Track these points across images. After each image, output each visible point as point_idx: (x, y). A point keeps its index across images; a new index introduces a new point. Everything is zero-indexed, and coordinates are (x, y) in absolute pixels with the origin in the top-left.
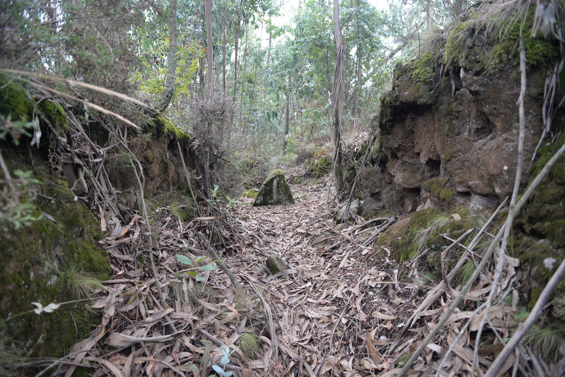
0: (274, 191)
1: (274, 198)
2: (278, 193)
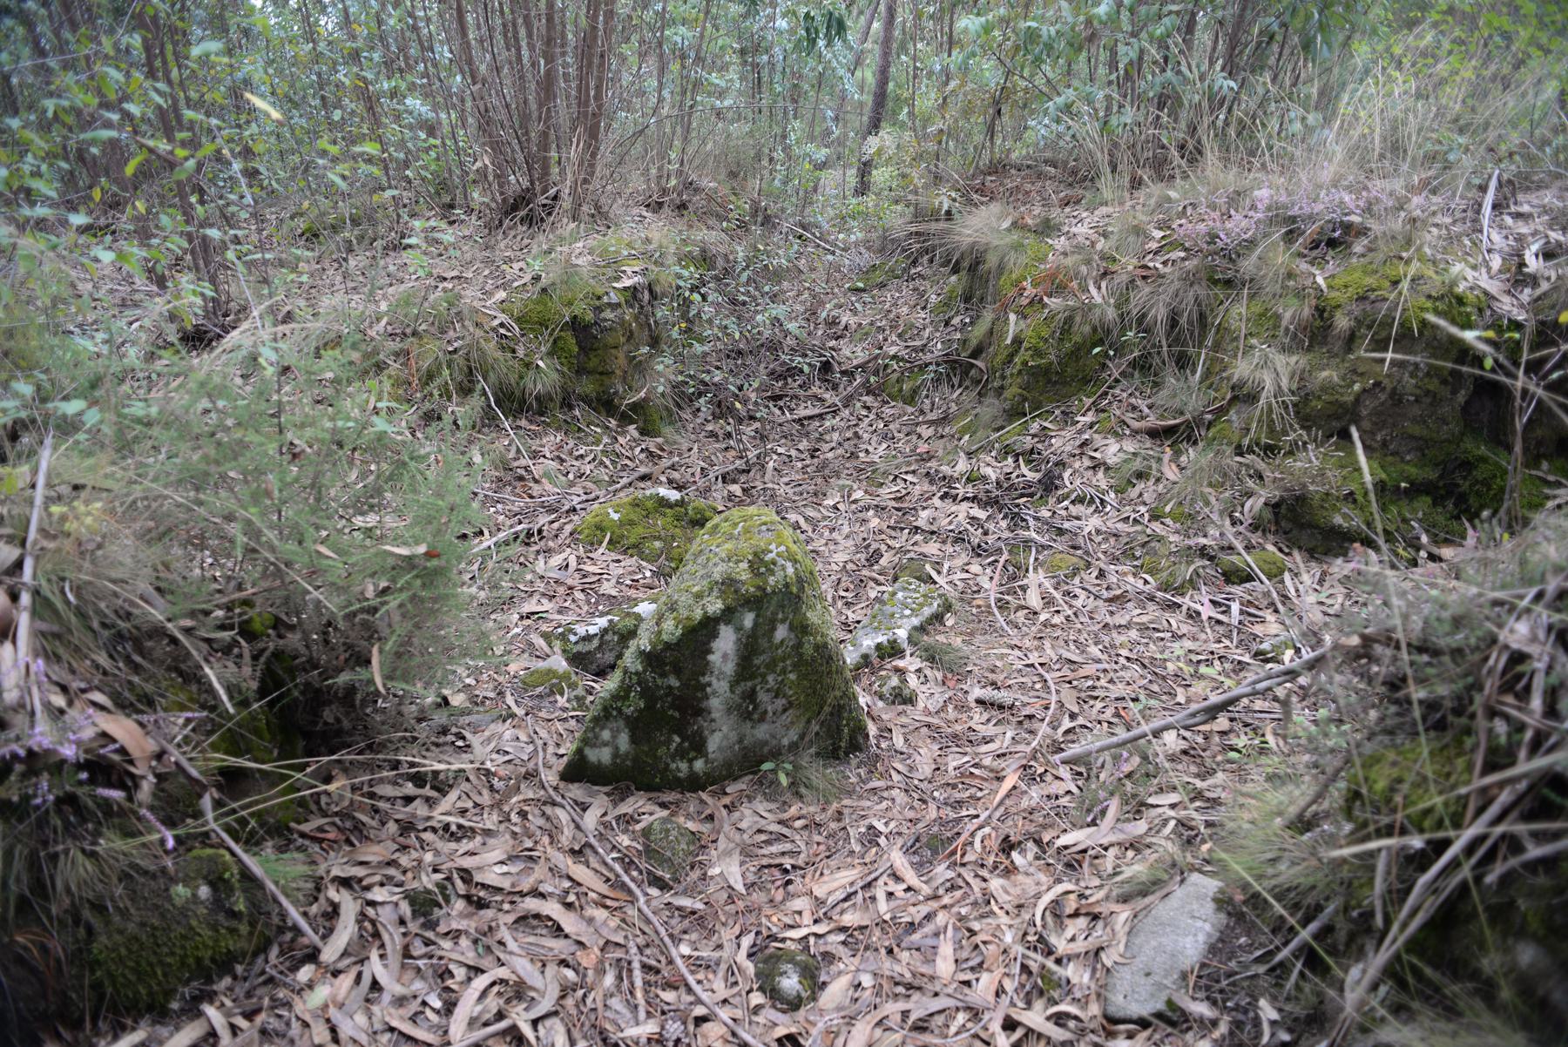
0: (715, 703)
1: (714, 743)
2: (747, 709)
